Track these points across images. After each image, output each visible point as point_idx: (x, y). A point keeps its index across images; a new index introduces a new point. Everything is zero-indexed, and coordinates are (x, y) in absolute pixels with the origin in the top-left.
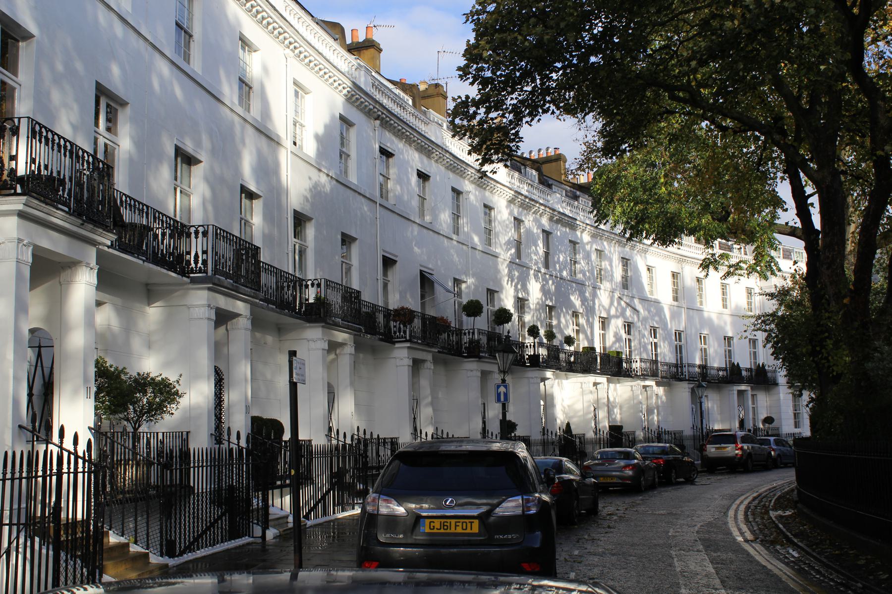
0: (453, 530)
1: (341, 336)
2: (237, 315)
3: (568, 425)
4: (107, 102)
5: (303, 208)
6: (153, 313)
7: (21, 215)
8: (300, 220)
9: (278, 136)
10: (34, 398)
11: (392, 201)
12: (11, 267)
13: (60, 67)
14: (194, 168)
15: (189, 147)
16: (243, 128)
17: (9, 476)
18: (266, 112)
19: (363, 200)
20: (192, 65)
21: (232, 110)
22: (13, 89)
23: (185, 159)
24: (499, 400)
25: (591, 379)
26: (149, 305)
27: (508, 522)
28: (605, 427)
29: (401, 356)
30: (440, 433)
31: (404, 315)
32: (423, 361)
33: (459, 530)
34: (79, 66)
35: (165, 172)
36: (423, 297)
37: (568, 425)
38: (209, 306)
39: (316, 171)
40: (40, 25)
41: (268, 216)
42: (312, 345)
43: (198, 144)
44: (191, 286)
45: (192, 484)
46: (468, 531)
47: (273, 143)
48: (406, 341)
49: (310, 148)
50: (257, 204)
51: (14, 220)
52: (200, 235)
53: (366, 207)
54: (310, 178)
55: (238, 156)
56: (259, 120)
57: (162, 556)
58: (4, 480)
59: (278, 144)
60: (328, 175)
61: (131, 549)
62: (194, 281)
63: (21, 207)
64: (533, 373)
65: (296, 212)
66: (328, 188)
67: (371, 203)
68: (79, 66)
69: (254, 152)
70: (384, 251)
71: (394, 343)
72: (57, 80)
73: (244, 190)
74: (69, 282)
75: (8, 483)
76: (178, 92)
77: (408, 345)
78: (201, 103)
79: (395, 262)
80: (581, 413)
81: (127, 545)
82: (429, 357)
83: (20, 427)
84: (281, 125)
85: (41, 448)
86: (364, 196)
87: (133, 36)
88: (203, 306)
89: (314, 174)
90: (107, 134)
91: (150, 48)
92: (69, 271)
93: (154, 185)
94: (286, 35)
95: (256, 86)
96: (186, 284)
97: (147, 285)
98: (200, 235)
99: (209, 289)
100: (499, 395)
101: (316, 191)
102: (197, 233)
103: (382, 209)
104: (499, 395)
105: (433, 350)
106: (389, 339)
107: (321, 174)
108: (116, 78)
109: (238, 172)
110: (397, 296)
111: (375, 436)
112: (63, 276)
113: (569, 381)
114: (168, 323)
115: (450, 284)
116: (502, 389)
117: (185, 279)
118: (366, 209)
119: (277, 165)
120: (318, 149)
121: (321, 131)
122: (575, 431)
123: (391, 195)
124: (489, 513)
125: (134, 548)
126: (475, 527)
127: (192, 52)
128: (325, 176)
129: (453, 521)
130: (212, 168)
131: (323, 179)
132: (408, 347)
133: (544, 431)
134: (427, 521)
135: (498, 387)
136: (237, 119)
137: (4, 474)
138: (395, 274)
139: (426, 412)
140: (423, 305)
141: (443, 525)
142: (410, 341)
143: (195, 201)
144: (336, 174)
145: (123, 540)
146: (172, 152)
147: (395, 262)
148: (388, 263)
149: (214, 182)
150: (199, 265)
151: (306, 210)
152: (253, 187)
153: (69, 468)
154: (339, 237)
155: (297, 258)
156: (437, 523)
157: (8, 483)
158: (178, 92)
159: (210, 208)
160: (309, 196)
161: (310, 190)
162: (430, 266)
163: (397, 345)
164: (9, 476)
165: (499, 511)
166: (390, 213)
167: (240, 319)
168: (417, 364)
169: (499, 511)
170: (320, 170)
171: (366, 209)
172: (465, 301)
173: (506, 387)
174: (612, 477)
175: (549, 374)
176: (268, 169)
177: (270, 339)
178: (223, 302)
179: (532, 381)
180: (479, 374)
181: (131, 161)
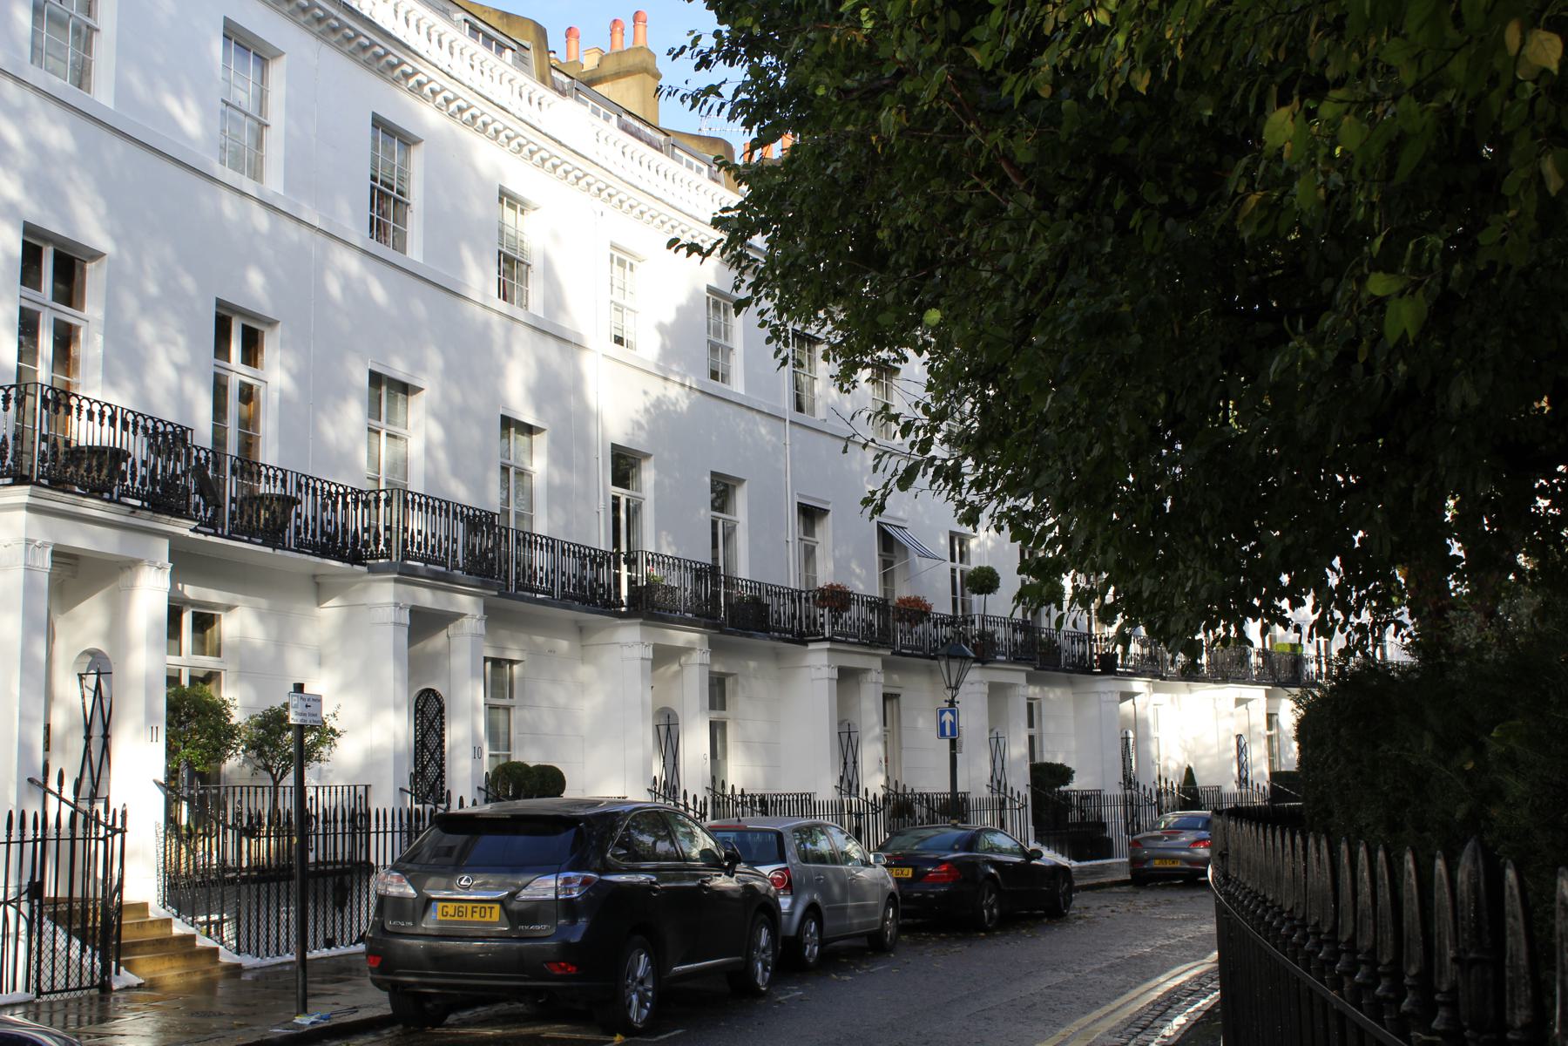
0: (469, 918)
1: (681, 637)
2: (459, 616)
3: (1189, 771)
4: (237, 331)
5: (630, 441)
6: (330, 612)
7: (30, 508)
8: (624, 465)
9: (579, 335)
10: (93, 741)
11: (821, 413)
12: (17, 576)
13: (152, 289)
14: (412, 399)
15: (399, 369)
16: (508, 331)
17: (15, 836)
18: (555, 300)
19: (758, 417)
20: (409, 254)
21: (484, 307)
22: (78, 328)
23: (387, 389)
24: (942, 734)
25: (1232, 691)
26: (319, 604)
27: (535, 912)
28: (1261, 774)
29: (818, 663)
30: (892, 786)
31: (837, 598)
32: (866, 671)
33: (476, 917)
34: (188, 283)
35: (354, 413)
36: (886, 564)
37: (1189, 771)
38: (396, 605)
39: (660, 381)
40: (117, 239)
41: (560, 456)
42: (626, 652)
43: (419, 365)
44: (371, 577)
45: (373, 860)
46: (487, 919)
47: (569, 347)
48: (825, 640)
49: (648, 346)
50: (540, 441)
51: (23, 515)
52: (382, 504)
53: (763, 428)
54: (645, 393)
55: (498, 372)
56: (541, 315)
57: (238, 952)
58: (8, 843)
59: (580, 346)
60: (683, 385)
61: (198, 943)
62: (373, 570)
63: (26, 499)
64: (1107, 686)
65: (614, 446)
66: (684, 405)
67: (774, 421)
68: (188, 283)
69: (532, 362)
70: (800, 496)
71: (805, 643)
72: (148, 307)
73: (507, 423)
74: (130, 588)
75: (14, 848)
76: (378, 293)
77: (827, 645)
78: (420, 304)
79: (826, 512)
80: (1215, 751)
81: (193, 937)
82: (876, 664)
83: (31, 780)
84: (587, 316)
85: (846, 799)
86: (759, 412)
87: (289, 226)
88: (387, 605)
89: (656, 388)
90: (244, 369)
91: (320, 238)
92: (128, 573)
93: (330, 432)
94: (588, 179)
95: (536, 263)
96: (360, 574)
97: (314, 576)
98: (382, 504)
99: (396, 581)
100: (943, 726)
101: (659, 412)
102: (377, 500)
103: (796, 428)
104: (943, 726)
105: (881, 652)
106: (803, 636)
107: (669, 384)
108: (255, 290)
109: (497, 396)
110: (831, 566)
111: (738, 792)
112: (123, 579)
113: (1194, 695)
114: (348, 629)
115: (944, 541)
116: (948, 717)
117: (357, 567)
118: (763, 431)
119: (578, 379)
120: (663, 347)
121: (669, 317)
122: (1202, 781)
123: (819, 405)
124: (512, 896)
125: (203, 942)
126: (496, 913)
127: (409, 229)
128: (677, 388)
129: (470, 906)
130: (445, 397)
131: (674, 391)
132: (829, 650)
133: (1128, 781)
134: (440, 905)
135: (942, 712)
136: (495, 317)
137: (9, 835)
138: (825, 532)
139: (870, 755)
140: (887, 578)
141: (458, 911)
142: (830, 640)
143: (415, 446)
144: (698, 381)
145: (190, 930)
146: (364, 380)
147: (826, 512)
148: (810, 515)
149: (448, 417)
150: (381, 547)
151: (639, 443)
152: (528, 417)
153: (23, 835)
154: (708, 480)
155: (623, 516)
156: (451, 908)
157: (14, 848)
158: (378, 293)
159: (441, 456)
160: (643, 422)
161: (647, 410)
162: (900, 514)
163: (812, 646)
164: (15, 836)
165: (525, 895)
166: (815, 435)
167: (465, 620)
168: (847, 677)
169: (525, 895)
170: (666, 379)
171: (763, 431)
172: (974, 564)
173: (953, 713)
174: (1174, 859)
175: (1138, 685)
176: (557, 389)
177: (563, 645)
178: (426, 598)
179: (1104, 697)
180: (986, 689)
181: (284, 400)
